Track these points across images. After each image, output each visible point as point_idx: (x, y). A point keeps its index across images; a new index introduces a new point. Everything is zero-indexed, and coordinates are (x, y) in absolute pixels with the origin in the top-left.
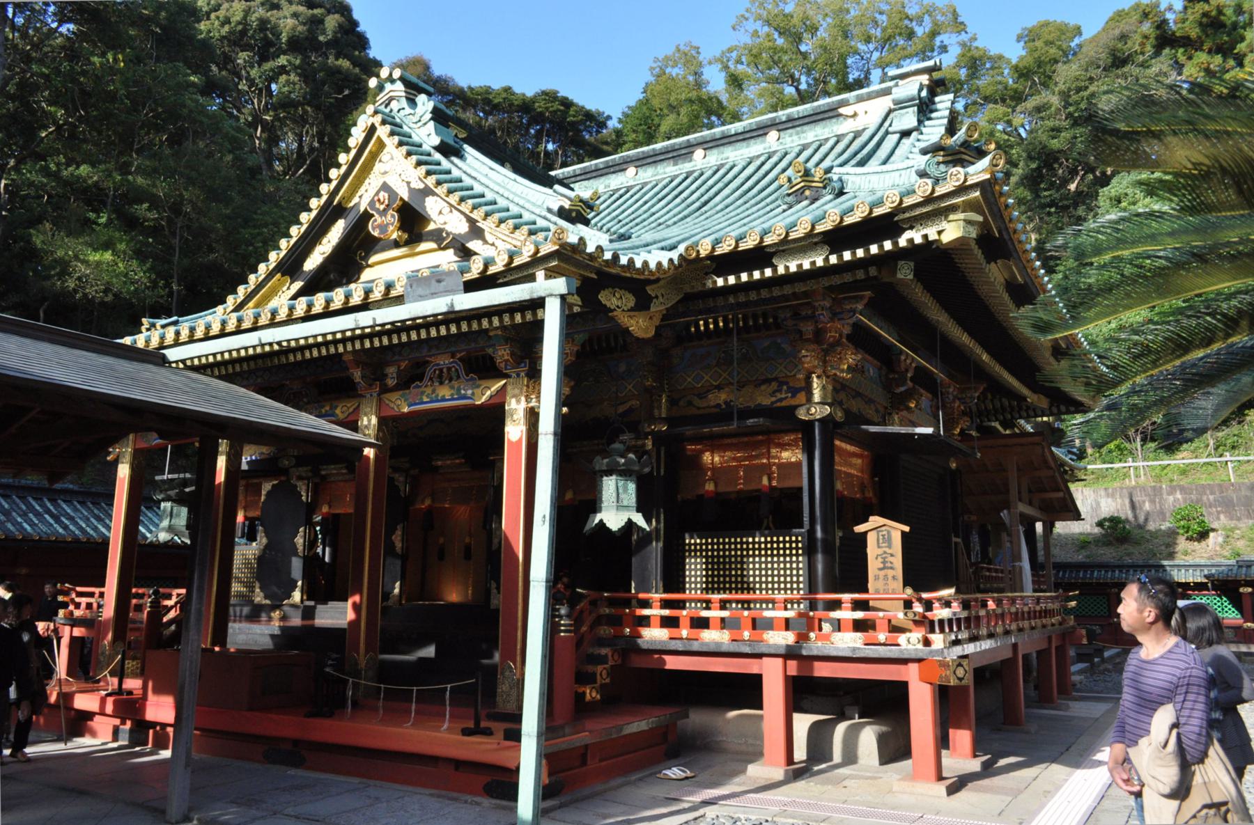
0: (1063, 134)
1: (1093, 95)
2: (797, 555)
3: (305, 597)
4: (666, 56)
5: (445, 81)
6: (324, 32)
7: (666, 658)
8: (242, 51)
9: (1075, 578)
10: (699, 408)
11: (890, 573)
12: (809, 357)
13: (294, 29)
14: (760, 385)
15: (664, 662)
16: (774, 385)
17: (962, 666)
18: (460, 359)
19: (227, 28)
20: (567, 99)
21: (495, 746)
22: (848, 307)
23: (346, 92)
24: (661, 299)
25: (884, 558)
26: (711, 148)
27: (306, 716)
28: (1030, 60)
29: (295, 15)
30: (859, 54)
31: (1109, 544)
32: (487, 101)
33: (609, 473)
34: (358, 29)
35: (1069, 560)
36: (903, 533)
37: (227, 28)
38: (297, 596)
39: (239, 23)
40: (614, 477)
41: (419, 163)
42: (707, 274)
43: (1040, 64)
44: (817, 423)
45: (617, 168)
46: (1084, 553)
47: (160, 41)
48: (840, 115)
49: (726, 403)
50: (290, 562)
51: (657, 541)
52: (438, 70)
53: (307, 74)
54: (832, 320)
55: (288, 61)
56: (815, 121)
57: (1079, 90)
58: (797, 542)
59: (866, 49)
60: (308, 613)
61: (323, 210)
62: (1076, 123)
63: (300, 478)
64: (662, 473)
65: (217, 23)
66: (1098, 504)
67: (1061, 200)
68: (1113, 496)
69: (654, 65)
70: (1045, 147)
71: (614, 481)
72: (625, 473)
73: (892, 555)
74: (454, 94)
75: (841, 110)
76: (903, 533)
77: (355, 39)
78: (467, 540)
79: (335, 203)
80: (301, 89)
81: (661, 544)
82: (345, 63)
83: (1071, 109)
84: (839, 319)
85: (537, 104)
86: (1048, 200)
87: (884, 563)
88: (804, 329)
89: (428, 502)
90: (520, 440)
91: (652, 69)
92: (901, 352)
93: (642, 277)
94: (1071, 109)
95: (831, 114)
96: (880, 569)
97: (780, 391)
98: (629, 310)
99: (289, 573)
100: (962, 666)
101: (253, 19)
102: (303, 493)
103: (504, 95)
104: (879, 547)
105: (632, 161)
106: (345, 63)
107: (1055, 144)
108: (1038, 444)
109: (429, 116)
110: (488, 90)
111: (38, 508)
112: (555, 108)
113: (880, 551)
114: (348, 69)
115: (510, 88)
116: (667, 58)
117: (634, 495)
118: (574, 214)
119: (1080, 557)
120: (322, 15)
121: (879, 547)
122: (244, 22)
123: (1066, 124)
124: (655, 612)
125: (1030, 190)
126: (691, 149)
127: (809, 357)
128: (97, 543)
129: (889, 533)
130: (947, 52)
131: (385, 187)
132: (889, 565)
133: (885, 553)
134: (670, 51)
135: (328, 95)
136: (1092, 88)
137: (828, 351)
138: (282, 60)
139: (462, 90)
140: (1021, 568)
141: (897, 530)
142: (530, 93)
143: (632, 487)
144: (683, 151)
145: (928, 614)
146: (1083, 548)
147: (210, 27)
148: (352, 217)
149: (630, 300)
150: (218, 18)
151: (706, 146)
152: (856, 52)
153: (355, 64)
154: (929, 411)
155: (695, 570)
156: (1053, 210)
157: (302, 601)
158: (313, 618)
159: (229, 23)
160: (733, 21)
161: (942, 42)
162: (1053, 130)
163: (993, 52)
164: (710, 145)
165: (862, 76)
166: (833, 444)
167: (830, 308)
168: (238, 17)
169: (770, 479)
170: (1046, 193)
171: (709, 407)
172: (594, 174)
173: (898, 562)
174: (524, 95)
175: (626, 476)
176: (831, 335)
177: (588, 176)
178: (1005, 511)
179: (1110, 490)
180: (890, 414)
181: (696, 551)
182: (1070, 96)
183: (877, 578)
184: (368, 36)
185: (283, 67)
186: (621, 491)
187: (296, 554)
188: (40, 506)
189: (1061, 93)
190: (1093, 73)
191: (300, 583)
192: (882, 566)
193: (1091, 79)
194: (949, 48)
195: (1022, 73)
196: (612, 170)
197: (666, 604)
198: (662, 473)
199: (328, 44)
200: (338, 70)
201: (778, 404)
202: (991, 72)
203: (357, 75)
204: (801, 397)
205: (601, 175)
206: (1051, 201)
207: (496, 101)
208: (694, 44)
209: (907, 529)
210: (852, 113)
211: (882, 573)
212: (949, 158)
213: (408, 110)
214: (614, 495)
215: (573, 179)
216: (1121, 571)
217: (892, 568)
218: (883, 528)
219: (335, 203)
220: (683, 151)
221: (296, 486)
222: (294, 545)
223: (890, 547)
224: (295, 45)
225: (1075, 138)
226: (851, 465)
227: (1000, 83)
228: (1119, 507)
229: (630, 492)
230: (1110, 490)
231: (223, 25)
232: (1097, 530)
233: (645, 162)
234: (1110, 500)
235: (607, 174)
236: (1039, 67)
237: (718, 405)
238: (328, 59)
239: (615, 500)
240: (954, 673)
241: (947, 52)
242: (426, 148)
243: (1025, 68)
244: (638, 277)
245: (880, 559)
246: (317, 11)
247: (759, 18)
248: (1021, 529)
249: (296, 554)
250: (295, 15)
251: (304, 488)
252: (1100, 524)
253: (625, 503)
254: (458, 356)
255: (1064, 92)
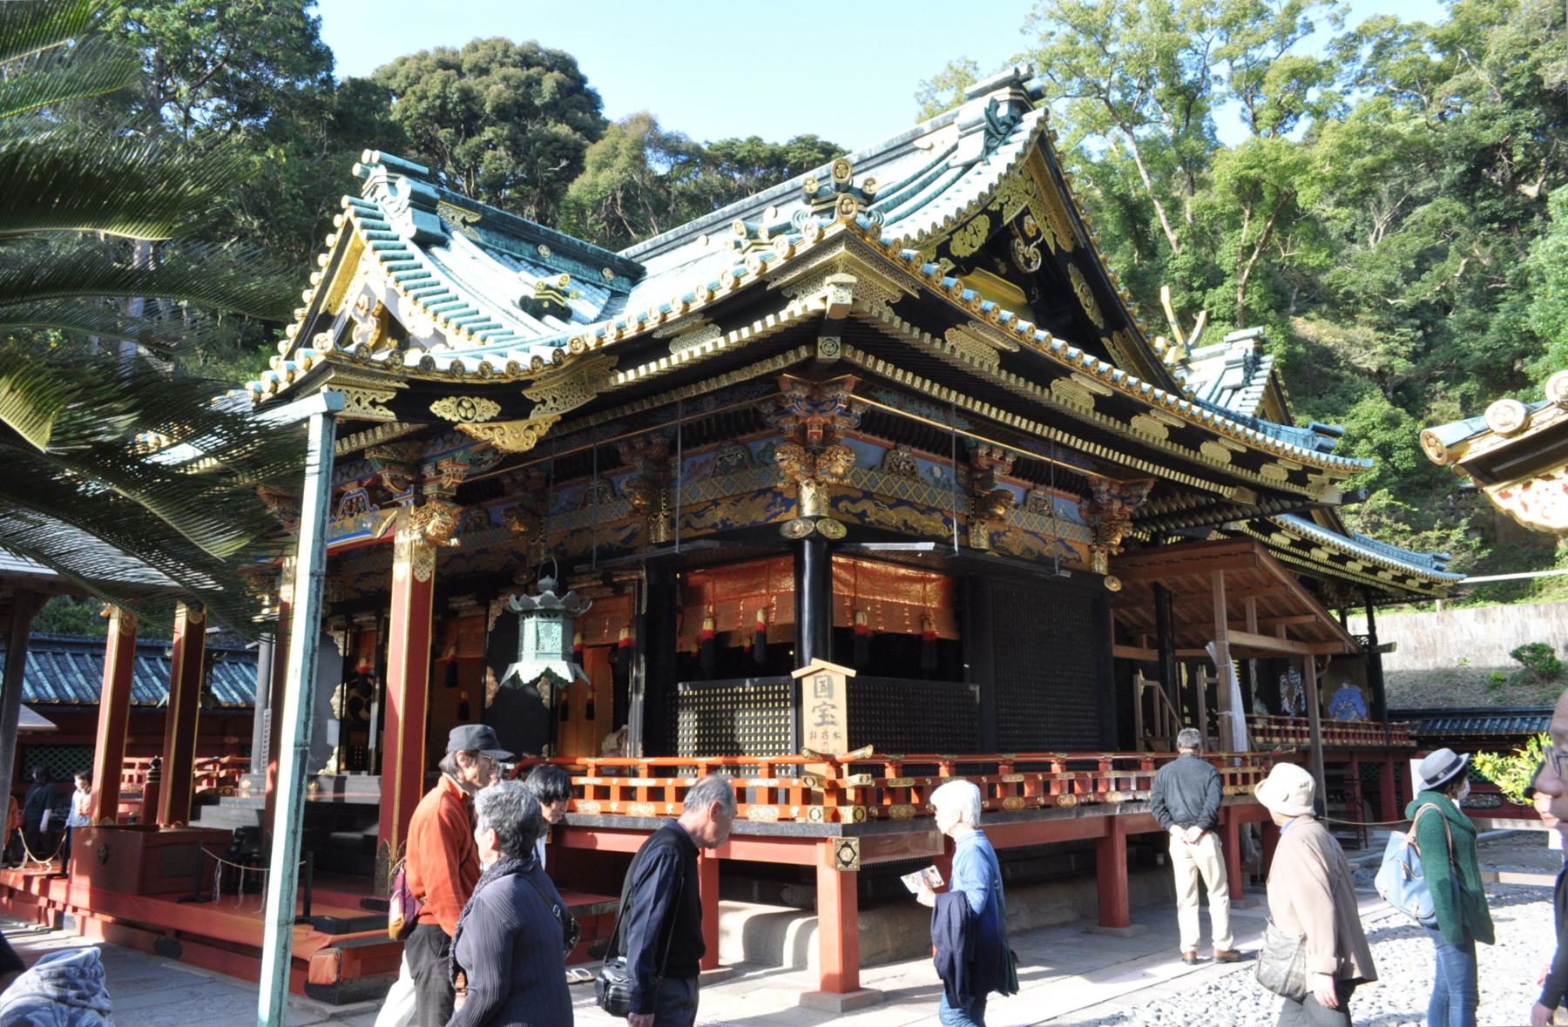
0: (1499, 122)
1: (1537, 64)
2: (786, 708)
3: (343, 766)
4: (936, 77)
5: (677, 138)
6: (540, 94)
7: (599, 836)
8: (442, 128)
9: (1457, 730)
10: (696, 530)
11: (831, 729)
12: (788, 461)
13: (499, 95)
14: (755, 497)
15: (595, 841)
16: (769, 495)
17: (850, 846)
18: (367, 487)
19: (424, 104)
20: (829, 144)
21: (304, 937)
22: (830, 396)
23: (564, 163)
24: (551, 404)
25: (823, 711)
26: (783, 203)
27: (179, 902)
28: (1455, 26)
29: (505, 79)
30: (1191, 47)
31: (1529, 682)
32: (730, 157)
33: (529, 612)
34: (587, 86)
35: (1474, 705)
36: (848, 678)
37: (424, 104)
38: (333, 764)
39: (438, 97)
40: (534, 619)
41: (384, 259)
42: (611, 369)
43: (1468, 28)
44: (807, 543)
45: (688, 238)
46: (1495, 694)
47: (333, 129)
48: (916, 149)
49: (723, 522)
50: (326, 725)
51: (637, 693)
52: (666, 127)
53: (517, 147)
54: (811, 412)
55: (494, 132)
56: (890, 160)
57: (1518, 58)
58: (786, 692)
59: (1200, 41)
60: (340, 784)
61: (308, 320)
62: (1519, 104)
63: (338, 629)
64: (644, 611)
65: (413, 99)
66: (1525, 627)
67: (1506, 211)
68: (1546, 614)
69: (920, 90)
70: (1475, 141)
71: (534, 625)
72: (547, 613)
73: (833, 707)
74: (686, 152)
75: (917, 143)
76: (848, 678)
77: (583, 98)
78: (590, 695)
79: (321, 312)
80: (509, 162)
81: (641, 697)
82: (563, 130)
83: (1508, 86)
84: (821, 412)
85: (791, 155)
86: (1488, 212)
87: (823, 716)
88: (786, 427)
89: (451, 652)
90: (430, 580)
91: (918, 95)
92: (978, 444)
93: (485, 382)
94: (1508, 86)
95: (906, 149)
96: (818, 725)
97: (773, 504)
98: (486, 421)
99: (325, 739)
100: (850, 846)
101: (453, 90)
102: (341, 647)
103: (749, 147)
104: (816, 696)
105: (701, 229)
106: (563, 130)
107: (1488, 137)
108: (1247, 552)
109: (407, 202)
110: (731, 144)
111: (147, 669)
112: (812, 158)
113: (818, 702)
114: (567, 135)
115: (756, 138)
116: (936, 80)
117: (559, 640)
118: (546, 305)
119: (1488, 702)
120: (539, 74)
121: (816, 696)
122: (443, 97)
123: (1501, 107)
124: (590, 781)
125: (1464, 201)
126: (762, 208)
127: (788, 461)
128: (224, 708)
129: (829, 678)
130: (1313, 31)
131: (367, 290)
132: (830, 719)
133: (825, 704)
134: (940, 69)
135: (544, 169)
136: (1536, 55)
137: (814, 451)
138: (488, 133)
139: (698, 148)
140: (1230, 719)
141: (839, 674)
142: (783, 143)
143: (557, 629)
144: (754, 211)
145: (839, 781)
146: (1493, 687)
147: (406, 104)
148: (339, 325)
149: (490, 408)
150: (414, 93)
151: (776, 202)
152: (1188, 46)
153: (576, 129)
154: (1079, 519)
155: (687, 724)
156: (1496, 225)
157: (339, 771)
158: (343, 791)
159: (427, 98)
160: (1021, 22)
161: (1305, 18)
162: (1484, 118)
163: (1406, 21)
164: (781, 200)
165: (1199, 76)
166: (829, 563)
167: (807, 398)
168: (436, 89)
169: (767, 613)
170: (1483, 204)
171: (706, 527)
172: (665, 248)
173: (841, 715)
174: (776, 144)
175: (549, 616)
176: (815, 432)
177: (660, 250)
178: (1211, 644)
179: (1542, 607)
180: (973, 524)
181: (690, 704)
182: (1504, 69)
183: (813, 736)
184: (600, 92)
185: (490, 141)
186: (541, 635)
187: (333, 717)
188: (150, 666)
189: (1492, 66)
190: (1538, 33)
191: (336, 750)
192: (820, 720)
193: (1536, 43)
194: (1316, 27)
195: (1447, 44)
196: (683, 241)
197: (656, 771)
198: (644, 611)
199: (546, 107)
200: (555, 138)
201: (773, 520)
202: (1404, 47)
203: (575, 141)
204: (794, 509)
205: (673, 248)
206: (1492, 213)
207: (739, 156)
208: (971, 59)
209: (852, 673)
210: (929, 145)
211: (820, 730)
212: (823, 207)
213: (390, 198)
214: (534, 640)
215: (645, 256)
216: (1524, 720)
217: (832, 723)
218: (822, 673)
219: (321, 312)
220: (754, 211)
221: (332, 638)
222: (331, 706)
223: (830, 696)
224: (503, 113)
225: (1518, 124)
226: (906, 594)
227: (1414, 61)
228: (1555, 631)
229: (555, 635)
230: (1542, 607)
231: (420, 99)
232: (1513, 662)
233: (715, 228)
234: (1542, 621)
235: (678, 246)
236: (1469, 33)
237: (714, 525)
238: (546, 124)
239: (534, 646)
240: (838, 855)
241: (1313, 31)
242: (401, 242)
243: (1447, 37)
244: (476, 382)
245: (818, 712)
246: (533, 71)
247: (1051, 16)
248: (1233, 666)
249: (333, 717)
250: (505, 79)
251: (341, 640)
252: (1516, 655)
253: (548, 650)
254: (366, 483)
255: (1495, 64)
